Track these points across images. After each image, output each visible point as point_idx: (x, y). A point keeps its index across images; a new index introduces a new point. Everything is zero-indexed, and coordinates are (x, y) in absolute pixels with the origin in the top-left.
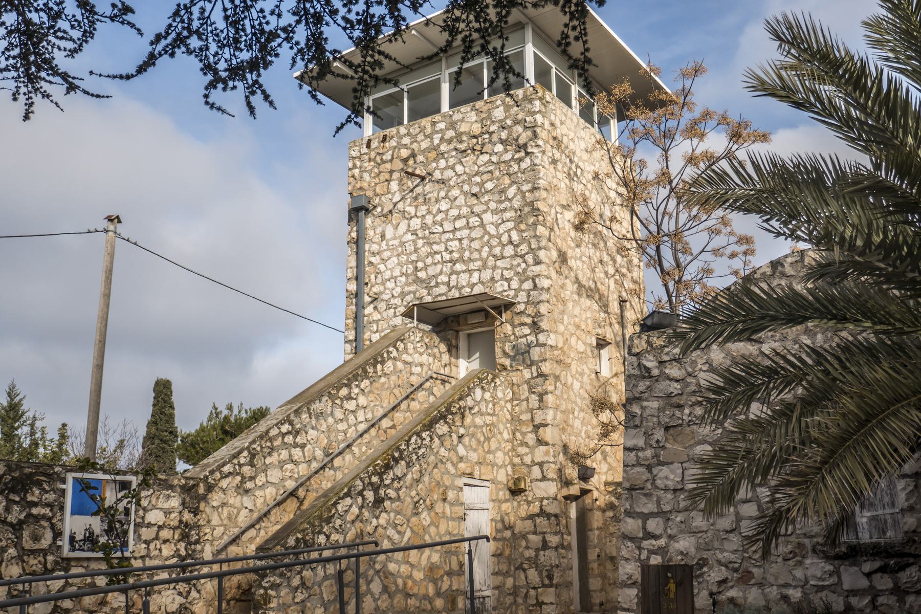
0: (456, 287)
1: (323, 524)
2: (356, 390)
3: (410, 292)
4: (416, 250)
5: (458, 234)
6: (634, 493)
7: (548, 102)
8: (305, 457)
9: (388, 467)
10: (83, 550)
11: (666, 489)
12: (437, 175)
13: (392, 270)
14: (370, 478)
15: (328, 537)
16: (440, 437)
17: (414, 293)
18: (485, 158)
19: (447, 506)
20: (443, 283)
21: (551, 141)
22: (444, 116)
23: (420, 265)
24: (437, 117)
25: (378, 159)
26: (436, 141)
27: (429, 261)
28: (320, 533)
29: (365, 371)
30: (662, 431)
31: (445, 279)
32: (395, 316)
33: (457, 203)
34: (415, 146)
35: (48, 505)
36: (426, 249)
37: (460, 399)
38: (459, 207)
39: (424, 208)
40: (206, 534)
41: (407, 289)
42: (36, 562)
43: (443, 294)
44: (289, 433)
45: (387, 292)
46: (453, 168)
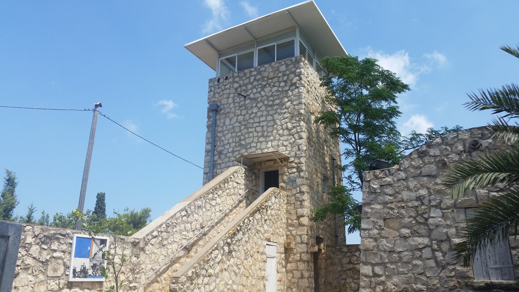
0: (260, 149)
1: (205, 264)
2: (216, 196)
3: (237, 151)
4: (240, 131)
5: (261, 124)
6: (367, 252)
7: (306, 64)
8: (192, 228)
9: (234, 234)
10: (80, 277)
11: (385, 251)
12: (252, 96)
13: (228, 140)
14: (227, 239)
15: (207, 271)
16: (257, 220)
17: (239, 151)
18: (276, 89)
19: (259, 255)
20: (253, 147)
21: (307, 82)
22: (256, 68)
23: (242, 138)
24: (252, 70)
25: (223, 87)
26: (252, 80)
27: (247, 136)
28: (203, 269)
29: (220, 186)
30: (382, 221)
31: (255, 145)
32: (229, 161)
33: (262, 109)
34: (241, 82)
35: (64, 252)
36: (246, 131)
37: (266, 202)
38: (262, 111)
39: (245, 111)
40: (143, 269)
41: (235, 149)
42: (54, 283)
43: (253, 152)
44: (185, 215)
45: (226, 150)
46: (260, 93)
